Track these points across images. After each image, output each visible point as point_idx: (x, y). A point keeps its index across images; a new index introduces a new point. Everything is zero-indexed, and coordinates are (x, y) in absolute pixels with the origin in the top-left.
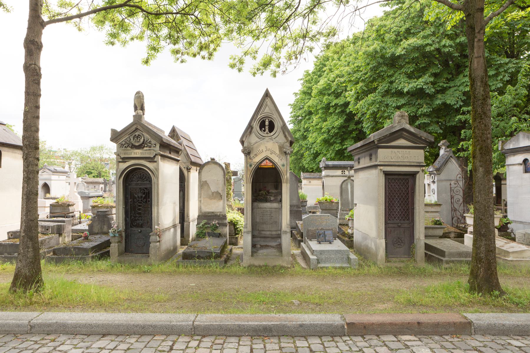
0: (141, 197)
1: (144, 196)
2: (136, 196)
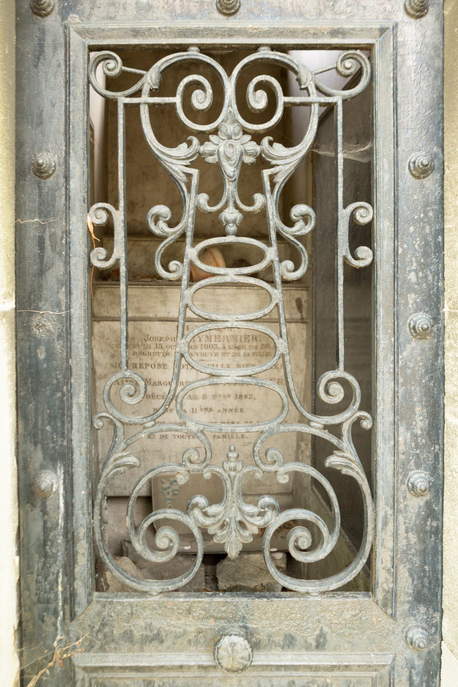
0: (252, 175)
1: (286, 160)
2: (176, 159)
